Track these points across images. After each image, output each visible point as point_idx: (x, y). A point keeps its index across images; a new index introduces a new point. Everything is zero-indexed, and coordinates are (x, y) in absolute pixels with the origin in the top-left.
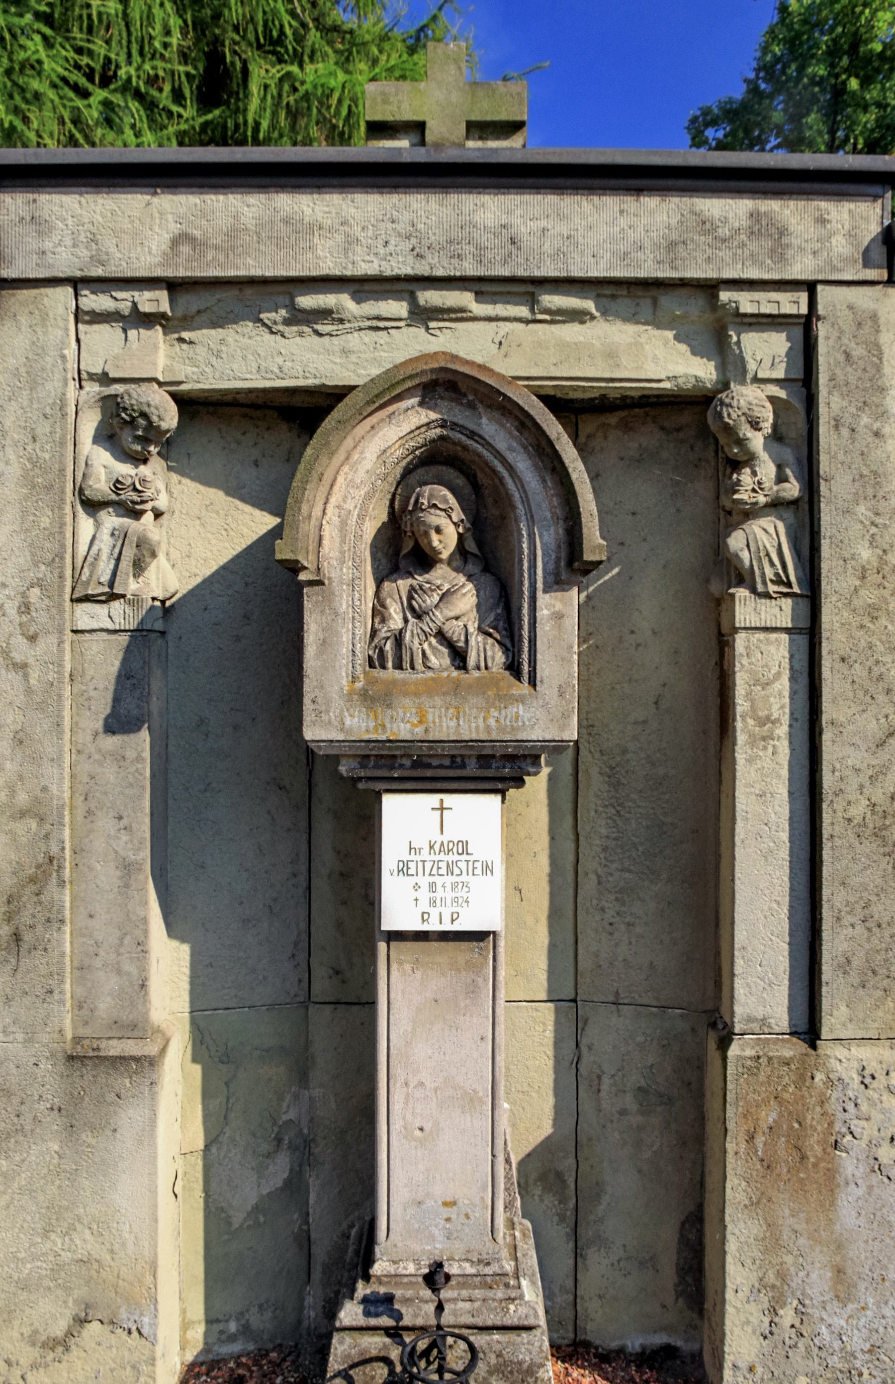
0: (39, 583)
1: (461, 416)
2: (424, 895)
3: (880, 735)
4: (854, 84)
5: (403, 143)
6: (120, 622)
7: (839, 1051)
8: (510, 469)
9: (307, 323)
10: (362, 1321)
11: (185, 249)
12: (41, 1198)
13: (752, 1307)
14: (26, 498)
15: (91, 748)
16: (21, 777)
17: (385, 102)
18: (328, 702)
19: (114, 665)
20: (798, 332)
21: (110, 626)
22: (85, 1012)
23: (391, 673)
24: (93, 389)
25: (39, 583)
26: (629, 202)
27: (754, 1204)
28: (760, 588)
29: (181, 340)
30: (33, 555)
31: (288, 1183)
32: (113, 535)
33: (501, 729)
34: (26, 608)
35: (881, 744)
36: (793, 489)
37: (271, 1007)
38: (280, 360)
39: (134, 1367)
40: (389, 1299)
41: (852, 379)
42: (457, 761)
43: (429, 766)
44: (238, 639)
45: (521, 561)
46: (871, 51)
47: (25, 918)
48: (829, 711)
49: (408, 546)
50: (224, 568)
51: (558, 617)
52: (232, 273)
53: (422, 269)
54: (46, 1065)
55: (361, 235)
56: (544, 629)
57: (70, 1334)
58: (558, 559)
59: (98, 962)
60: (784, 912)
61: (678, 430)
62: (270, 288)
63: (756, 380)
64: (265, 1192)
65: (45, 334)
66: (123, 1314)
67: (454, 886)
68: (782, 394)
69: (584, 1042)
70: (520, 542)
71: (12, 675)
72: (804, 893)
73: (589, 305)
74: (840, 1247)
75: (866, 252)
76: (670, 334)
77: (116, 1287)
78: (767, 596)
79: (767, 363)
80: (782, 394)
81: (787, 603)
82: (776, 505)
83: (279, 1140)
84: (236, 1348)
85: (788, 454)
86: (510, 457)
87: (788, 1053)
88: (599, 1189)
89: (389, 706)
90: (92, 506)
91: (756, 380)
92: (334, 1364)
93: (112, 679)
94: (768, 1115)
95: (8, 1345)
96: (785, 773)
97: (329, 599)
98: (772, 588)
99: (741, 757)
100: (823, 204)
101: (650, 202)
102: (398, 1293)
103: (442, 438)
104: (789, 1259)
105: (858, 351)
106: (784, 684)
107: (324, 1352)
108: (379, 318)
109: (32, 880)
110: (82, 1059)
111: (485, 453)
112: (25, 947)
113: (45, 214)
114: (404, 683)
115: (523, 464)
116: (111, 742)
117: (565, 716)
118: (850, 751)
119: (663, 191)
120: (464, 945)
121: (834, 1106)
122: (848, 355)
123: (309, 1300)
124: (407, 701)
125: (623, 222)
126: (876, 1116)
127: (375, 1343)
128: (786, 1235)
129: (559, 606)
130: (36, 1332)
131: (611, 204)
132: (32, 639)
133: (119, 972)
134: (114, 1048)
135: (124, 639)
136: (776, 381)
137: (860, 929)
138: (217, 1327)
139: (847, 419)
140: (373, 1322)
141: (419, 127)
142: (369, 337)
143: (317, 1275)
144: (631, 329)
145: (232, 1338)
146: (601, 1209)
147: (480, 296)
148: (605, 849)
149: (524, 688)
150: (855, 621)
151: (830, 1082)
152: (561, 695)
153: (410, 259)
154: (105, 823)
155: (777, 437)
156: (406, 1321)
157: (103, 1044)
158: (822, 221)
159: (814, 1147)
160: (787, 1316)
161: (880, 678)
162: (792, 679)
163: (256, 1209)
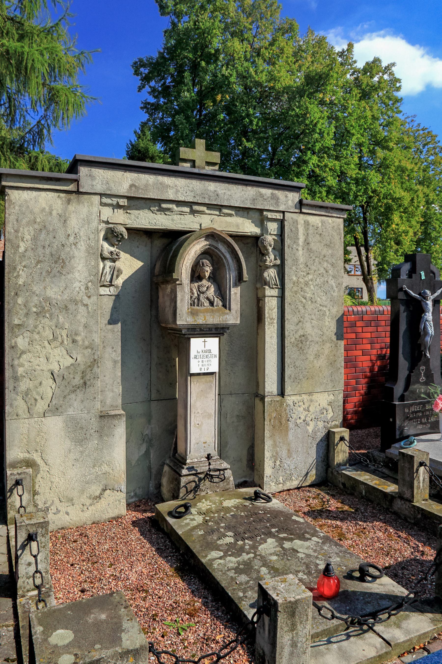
0: (91, 281)
1: (214, 244)
2: (201, 363)
3: (297, 322)
4: (203, 64)
5: (188, 165)
6: (112, 293)
7: (289, 398)
8: (225, 257)
9: (163, 211)
10: (188, 473)
11: (133, 188)
12: (92, 457)
13: (271, 462)
14: (87, 256)
15: (104, 328)
16: (86, 337)
17: (185, 153)
18: (183, 314)
19: (111, 304)
20: (280, 223)
21: (110, 294)
22: (103, 403)
23: (196, 307)
24: (103, 225)
25: (91, 281)
26: (244, 188)
27: (271, 436)
28: (271, 286)
29: (127, 212)
30: (89, 273)
31: (146, 451)
32: (110, 267)
33: (223, 321)
34: (87, 288)
35: (297, 324)
36: (278, 262)
37: (141, 402)
38: (155, 221)
39: (119, 501)
40: (193, 467)
41: (292, 236)
42: (210, 329)
43: (204, 331)
44: (133, 297)
45: (227, 280)
46: (210, 52)
47: (88, 377)
48: (287, 316)
49: (197, 275)
50: (130, 277)
51: (236, 294)
52: (146, 197)
53: (195, 201)
54: (93, 419)
55: (180, 190)
56: (233, 297)
57: (101, 494)
58: (236, 280)
59: (107, 389)
60: (276, 366)
61: (247, 244)
62: (154, 201)
63: (270, 234)
64: (140, 455)
65: (92, 209)
66: (116, 486)
67: (208, 361)
68: (276, 238)
69: (222, 405)
70: (226, 275)
71: (83, 308)
72: (280, 361)
73: (233, 213)
74: (289, 445)
75: (296, 205)
76: (250, 221)
77: (114, 479)
78: (273, 288)
79: (273, 230)
80: (276, 238)
81: (277, 290)
82: (275, 266)
83: (144, 440)
84: (133, 500)
85: (277, 253)
86: (225, 254)
87: (278, 399)
88: (227, 443)
89: (197, 316)
90: (103, 259)
91: (270, 234)
92: (182, 484)
93: (110, 308)
94: (274, 415)
95: (82, 500)
96: (276, 331)
97: (183, 289)
98: (274, 286)
99: (266, 328)
100: (287, 193)
101: (249, 188)
102: (195, 466)
103: (209, 248)
104: (278, 449)
105: (293, 229)
106: (276, 310)
107: (179, 482)
108: (182, 212)
109: (90, 366)
110: (104, 416)
111: (219, 253)
112: (87, 386)
113: (94, 174)
114: (200, 310)
115: (228, 256)
116: (110, 327)
117: (237, 318)
118: (291, 326)
119: (253, 186)
120: (209, 376)
121: (288, 411)
122: (291, 230)
123: (151, 485)
124: (201, 314)
125: (243, 193)
126: (297, 413)
127: (191, 478)
128: (278, 443)
129: (236, 291)
130: (91, 495)
131: (240, 187)
132: (89, 297)
133: (113, 392)
134: (113, 413)
135: (113, 297)
136: (275, 235)
137: (293, 368)
138: (128, 494)
139: (291, 246)
140: (191, 473)
141: (194, 162)
142: (179, 216)
143: (153, 477)
144: (242, 219)
145: (132, 497)
146: (227, 449)
147: (208, 208)
148: (228, 354)
149: (227, 311)
150: (292, 294)
151: (287, 406)
152: (236, 312)
153: (192, 198)
154: (109, 350)
155: (274, 249)
156: (199, 471)
157: (109, 412)
158: (286, 197)
159: (284, 421)
160: (278, 463)
161: (297, 308)
162: (278, 309)
163: (138, 460)
